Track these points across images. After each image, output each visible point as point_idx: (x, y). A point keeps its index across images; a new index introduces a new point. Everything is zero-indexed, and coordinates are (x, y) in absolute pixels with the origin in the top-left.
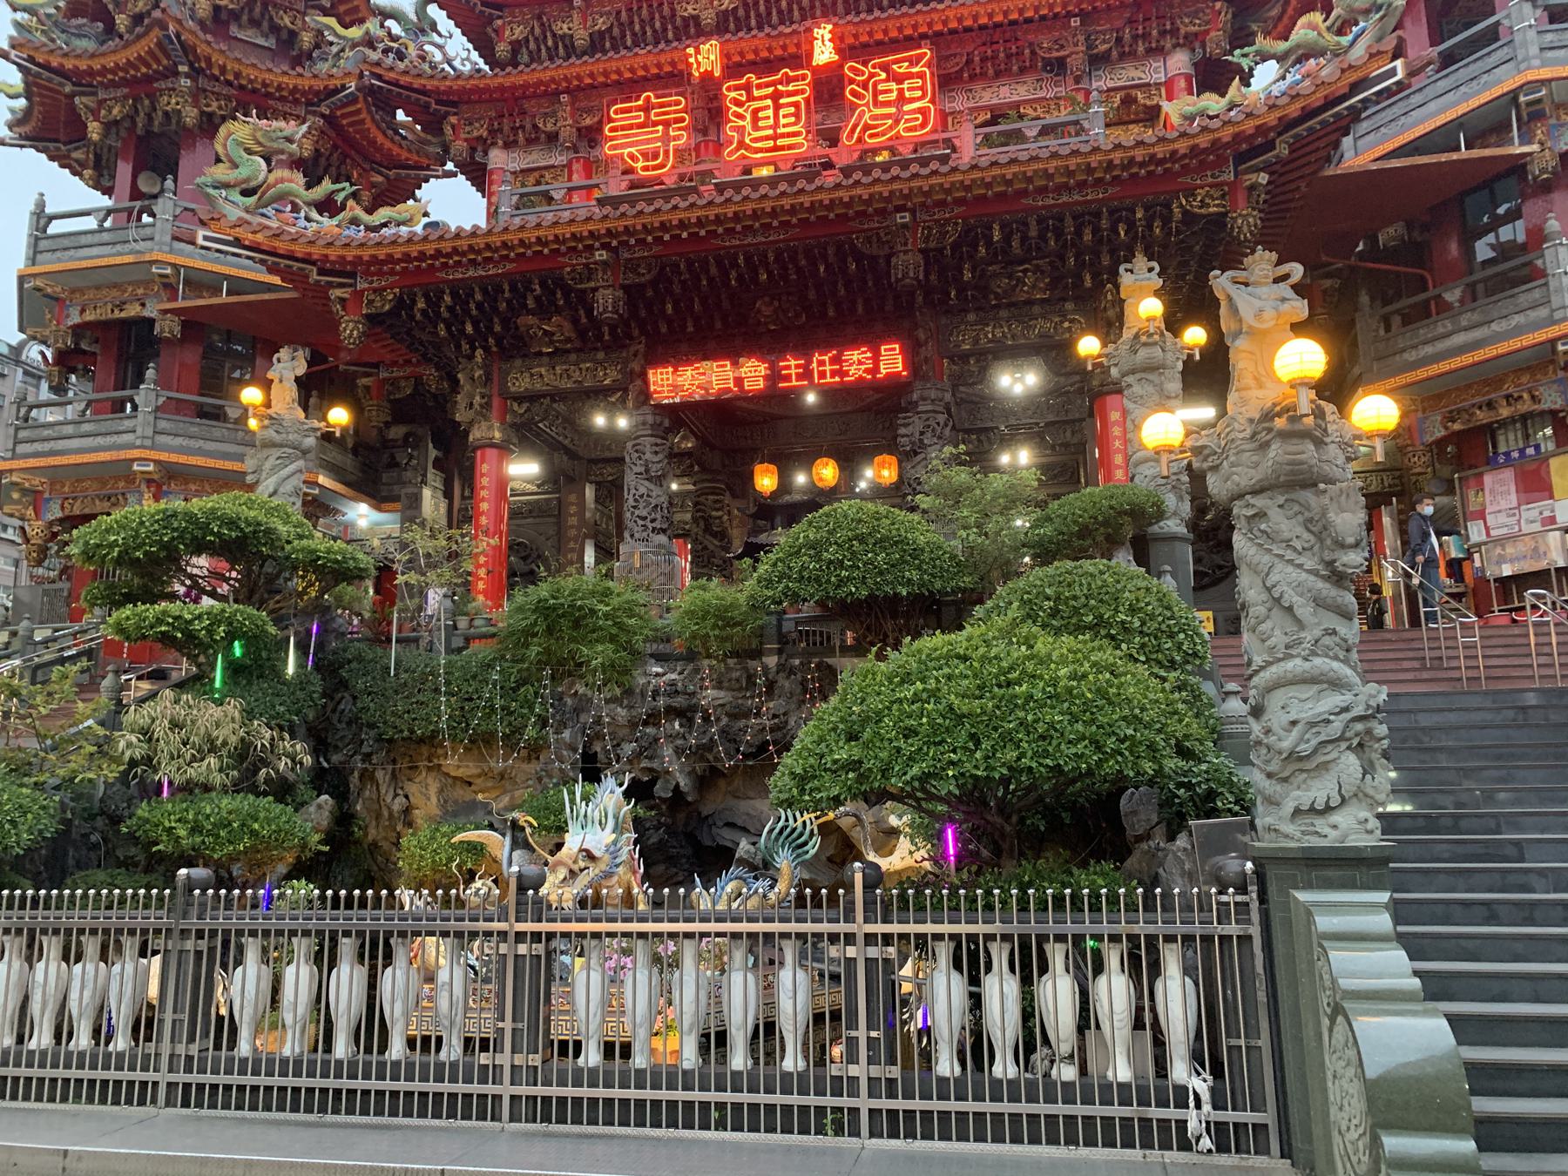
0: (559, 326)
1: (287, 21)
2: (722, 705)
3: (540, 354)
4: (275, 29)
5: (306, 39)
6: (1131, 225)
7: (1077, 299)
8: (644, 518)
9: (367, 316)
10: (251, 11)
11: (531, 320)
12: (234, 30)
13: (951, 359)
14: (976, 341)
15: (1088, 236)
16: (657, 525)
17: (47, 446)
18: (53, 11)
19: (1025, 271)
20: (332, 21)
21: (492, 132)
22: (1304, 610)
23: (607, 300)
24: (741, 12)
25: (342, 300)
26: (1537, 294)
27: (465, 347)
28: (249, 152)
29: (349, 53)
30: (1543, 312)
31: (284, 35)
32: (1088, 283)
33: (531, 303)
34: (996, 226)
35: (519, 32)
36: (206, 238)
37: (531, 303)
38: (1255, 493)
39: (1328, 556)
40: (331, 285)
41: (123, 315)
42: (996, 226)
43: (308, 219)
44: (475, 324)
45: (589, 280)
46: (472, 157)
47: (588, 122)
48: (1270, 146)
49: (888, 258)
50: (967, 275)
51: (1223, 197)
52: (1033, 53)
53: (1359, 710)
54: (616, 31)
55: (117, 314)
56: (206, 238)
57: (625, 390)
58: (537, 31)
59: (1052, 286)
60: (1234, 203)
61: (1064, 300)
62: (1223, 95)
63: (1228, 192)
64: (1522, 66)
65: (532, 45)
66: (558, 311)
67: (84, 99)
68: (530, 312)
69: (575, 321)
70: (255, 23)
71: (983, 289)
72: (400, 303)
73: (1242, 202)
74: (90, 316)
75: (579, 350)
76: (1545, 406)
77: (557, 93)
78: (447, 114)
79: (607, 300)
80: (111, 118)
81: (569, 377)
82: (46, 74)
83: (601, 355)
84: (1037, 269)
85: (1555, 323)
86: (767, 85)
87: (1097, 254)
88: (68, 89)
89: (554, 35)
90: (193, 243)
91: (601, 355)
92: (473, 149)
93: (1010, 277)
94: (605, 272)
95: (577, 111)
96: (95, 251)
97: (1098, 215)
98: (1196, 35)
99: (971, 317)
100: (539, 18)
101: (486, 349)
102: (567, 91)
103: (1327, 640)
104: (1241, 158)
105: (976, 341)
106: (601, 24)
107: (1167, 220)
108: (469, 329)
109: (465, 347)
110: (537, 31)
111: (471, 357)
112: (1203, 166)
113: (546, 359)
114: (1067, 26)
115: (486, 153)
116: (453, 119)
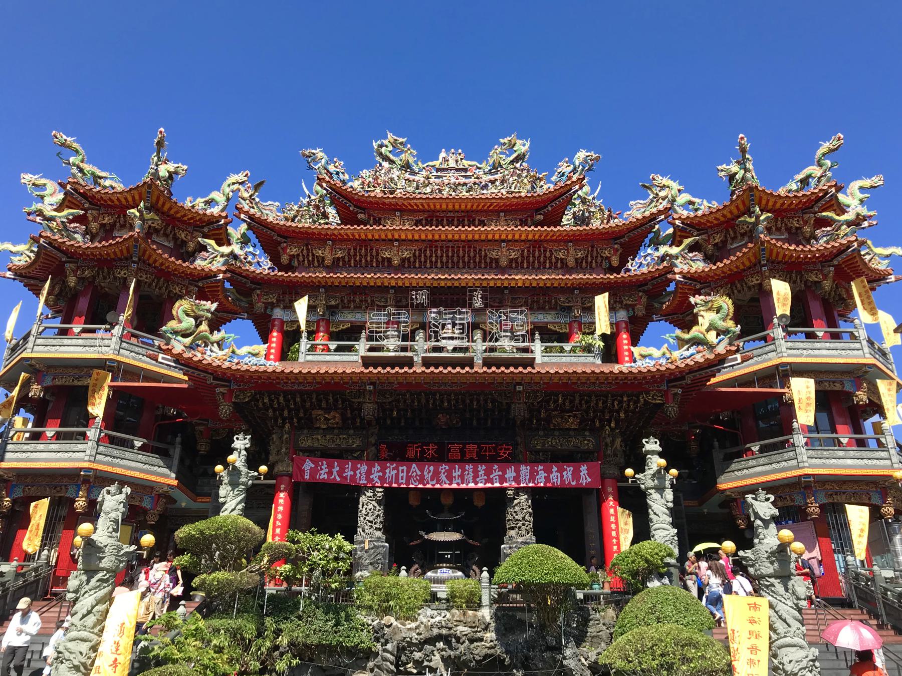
0: (335, 417)
1: (183, 236)
2: (466, 635)
3: (319, 428)
4: (175, 239)
5: (191, 246)
6: (621, 402)
7: (591, 430)
8: (371, 522)
9: (234, 403)
10: (165, 230)
11: (320, 412)
12: (154, 237)
13: (531, 452)
14: (544, 445)
15: (600, 405)
16: (377, 526)
17: (25, 455)
18: (65, 220)
19: (569, 416)
20: (212, 242)
21: (278, 301)
22: (790, 621)
23: (369, 409)
24: (412, 260)
25: (223, 394)
26: (791, 454)
27: (280, 421)
28: (188, 315)
29: (218, 258)
30: (794, 462)
31: (179, 242)
32: (597, 424)
33: (324, 405)
34: (560, 396)
35: (294, 251)
36: (163, 358)
37: (324, 405)
38: (770, 577)
39: (795, 602)
40: (217, 386)
41: (80, 383)
42: (560, 396)
43: (212, 351)
44: (289, 412)
45: (359, 397)
46: (265, 310)
47: (333, 303)
48: (683, 378)
49: (509, 405)
50: (543, 415)
51: (661, 396)
52: (556, 302)
53: (811, 657)
54: (347, 259)
55: (76, 383)
56: (163, 358)
57: (363, 451)
58: (305, 252)
59: (580, 423)
60: (667, 401)
61: (585, 430)
62: (659, 349)
63: (665, 394)
64: (780, 355)
65: (301, 258)
66: (336, 409)
67: (71, 265)
68: (321, 408)
69: (343, 415)
70: (166, 235)
71: (548, 420)
72: (254, 398)
73: (671, 400)
74: (58, 383)
75: (339, 428)
76: (796, 503)
77: (319, 287)
78: (255, 289)
79: (369, 409)
80: (83, 276)
81: (333, 441)
82: (55, 252)
83: (351, 432)
84: (575, 416)
85: (799, 468)
86: (449, 313)
87: (603, 412)
88: (64, 259)
89: (313, 255)
90: (156, 360)
91: (351, 432)
92: (266, 308)
93: (562, 418)
94: (370, 395)
95: (328, 298)
96: (72, 349)
97: (607, 397)
98: (630, 305)
99: (541, 433)
100: (307, 245)
101: (291, 423)
102: (324, 287)
103: (798, 632)
104: (669, 381)
105: (544, 445)
106: (339, 254)
107: (637, 401)
108: (286, 413)
109: (280, 421)
110: (305, 252)
111: (283, 427)
112: (655, 382)
113: (321, 431)
114: (573, 293)
115: (272, 309)
116: (258, 292)
